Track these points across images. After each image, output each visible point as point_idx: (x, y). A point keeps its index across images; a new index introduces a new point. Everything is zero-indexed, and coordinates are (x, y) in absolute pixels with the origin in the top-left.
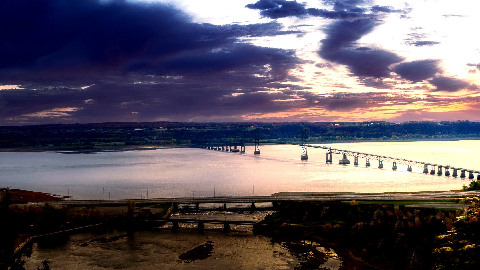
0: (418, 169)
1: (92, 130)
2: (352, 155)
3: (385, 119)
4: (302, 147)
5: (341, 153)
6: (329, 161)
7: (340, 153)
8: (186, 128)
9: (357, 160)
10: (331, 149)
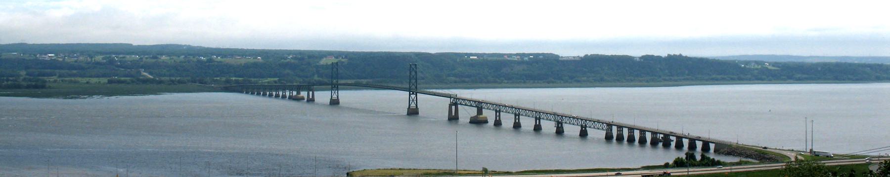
0: (596, 134)
1: (50, 55)
2: (486, 107)
4: (410, 94)
6: (453, 118)
8: (217, 57)
10: (457, 99)
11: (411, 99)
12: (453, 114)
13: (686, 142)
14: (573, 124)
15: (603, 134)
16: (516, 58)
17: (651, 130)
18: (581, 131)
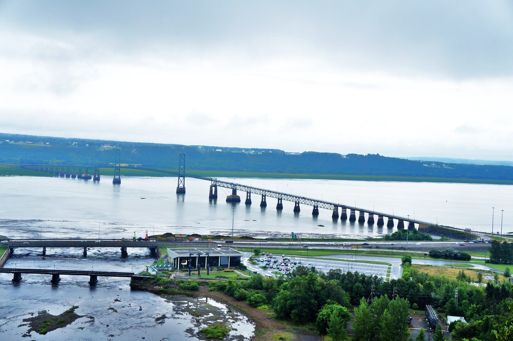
0: (325, 214)
3: (501, 162)
5: (230, 187)
6: (213, 197)
7: (220, 185)
9: (250, 196)
11: (183, 183)
12: (213, 193)
13: (396, 222)
14: (290, 201)
15: (331, 212)
16: (252, 152)
17: (351, 208)
18: (314, 210)
